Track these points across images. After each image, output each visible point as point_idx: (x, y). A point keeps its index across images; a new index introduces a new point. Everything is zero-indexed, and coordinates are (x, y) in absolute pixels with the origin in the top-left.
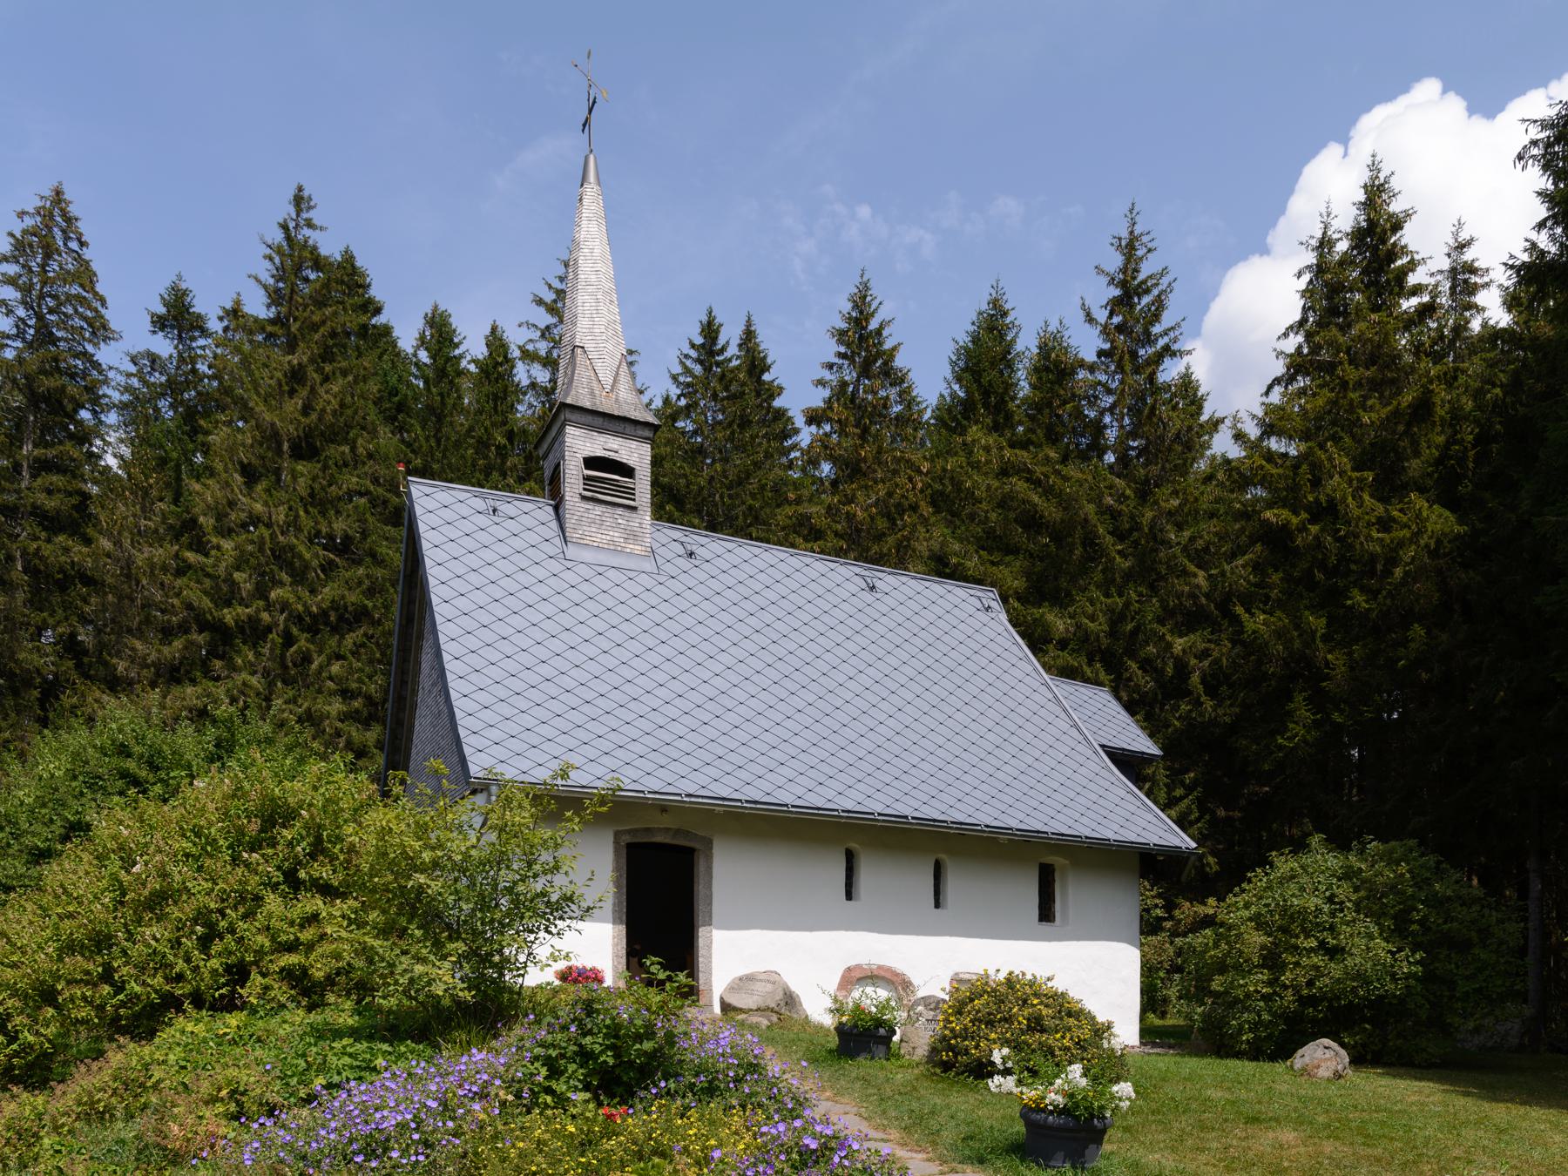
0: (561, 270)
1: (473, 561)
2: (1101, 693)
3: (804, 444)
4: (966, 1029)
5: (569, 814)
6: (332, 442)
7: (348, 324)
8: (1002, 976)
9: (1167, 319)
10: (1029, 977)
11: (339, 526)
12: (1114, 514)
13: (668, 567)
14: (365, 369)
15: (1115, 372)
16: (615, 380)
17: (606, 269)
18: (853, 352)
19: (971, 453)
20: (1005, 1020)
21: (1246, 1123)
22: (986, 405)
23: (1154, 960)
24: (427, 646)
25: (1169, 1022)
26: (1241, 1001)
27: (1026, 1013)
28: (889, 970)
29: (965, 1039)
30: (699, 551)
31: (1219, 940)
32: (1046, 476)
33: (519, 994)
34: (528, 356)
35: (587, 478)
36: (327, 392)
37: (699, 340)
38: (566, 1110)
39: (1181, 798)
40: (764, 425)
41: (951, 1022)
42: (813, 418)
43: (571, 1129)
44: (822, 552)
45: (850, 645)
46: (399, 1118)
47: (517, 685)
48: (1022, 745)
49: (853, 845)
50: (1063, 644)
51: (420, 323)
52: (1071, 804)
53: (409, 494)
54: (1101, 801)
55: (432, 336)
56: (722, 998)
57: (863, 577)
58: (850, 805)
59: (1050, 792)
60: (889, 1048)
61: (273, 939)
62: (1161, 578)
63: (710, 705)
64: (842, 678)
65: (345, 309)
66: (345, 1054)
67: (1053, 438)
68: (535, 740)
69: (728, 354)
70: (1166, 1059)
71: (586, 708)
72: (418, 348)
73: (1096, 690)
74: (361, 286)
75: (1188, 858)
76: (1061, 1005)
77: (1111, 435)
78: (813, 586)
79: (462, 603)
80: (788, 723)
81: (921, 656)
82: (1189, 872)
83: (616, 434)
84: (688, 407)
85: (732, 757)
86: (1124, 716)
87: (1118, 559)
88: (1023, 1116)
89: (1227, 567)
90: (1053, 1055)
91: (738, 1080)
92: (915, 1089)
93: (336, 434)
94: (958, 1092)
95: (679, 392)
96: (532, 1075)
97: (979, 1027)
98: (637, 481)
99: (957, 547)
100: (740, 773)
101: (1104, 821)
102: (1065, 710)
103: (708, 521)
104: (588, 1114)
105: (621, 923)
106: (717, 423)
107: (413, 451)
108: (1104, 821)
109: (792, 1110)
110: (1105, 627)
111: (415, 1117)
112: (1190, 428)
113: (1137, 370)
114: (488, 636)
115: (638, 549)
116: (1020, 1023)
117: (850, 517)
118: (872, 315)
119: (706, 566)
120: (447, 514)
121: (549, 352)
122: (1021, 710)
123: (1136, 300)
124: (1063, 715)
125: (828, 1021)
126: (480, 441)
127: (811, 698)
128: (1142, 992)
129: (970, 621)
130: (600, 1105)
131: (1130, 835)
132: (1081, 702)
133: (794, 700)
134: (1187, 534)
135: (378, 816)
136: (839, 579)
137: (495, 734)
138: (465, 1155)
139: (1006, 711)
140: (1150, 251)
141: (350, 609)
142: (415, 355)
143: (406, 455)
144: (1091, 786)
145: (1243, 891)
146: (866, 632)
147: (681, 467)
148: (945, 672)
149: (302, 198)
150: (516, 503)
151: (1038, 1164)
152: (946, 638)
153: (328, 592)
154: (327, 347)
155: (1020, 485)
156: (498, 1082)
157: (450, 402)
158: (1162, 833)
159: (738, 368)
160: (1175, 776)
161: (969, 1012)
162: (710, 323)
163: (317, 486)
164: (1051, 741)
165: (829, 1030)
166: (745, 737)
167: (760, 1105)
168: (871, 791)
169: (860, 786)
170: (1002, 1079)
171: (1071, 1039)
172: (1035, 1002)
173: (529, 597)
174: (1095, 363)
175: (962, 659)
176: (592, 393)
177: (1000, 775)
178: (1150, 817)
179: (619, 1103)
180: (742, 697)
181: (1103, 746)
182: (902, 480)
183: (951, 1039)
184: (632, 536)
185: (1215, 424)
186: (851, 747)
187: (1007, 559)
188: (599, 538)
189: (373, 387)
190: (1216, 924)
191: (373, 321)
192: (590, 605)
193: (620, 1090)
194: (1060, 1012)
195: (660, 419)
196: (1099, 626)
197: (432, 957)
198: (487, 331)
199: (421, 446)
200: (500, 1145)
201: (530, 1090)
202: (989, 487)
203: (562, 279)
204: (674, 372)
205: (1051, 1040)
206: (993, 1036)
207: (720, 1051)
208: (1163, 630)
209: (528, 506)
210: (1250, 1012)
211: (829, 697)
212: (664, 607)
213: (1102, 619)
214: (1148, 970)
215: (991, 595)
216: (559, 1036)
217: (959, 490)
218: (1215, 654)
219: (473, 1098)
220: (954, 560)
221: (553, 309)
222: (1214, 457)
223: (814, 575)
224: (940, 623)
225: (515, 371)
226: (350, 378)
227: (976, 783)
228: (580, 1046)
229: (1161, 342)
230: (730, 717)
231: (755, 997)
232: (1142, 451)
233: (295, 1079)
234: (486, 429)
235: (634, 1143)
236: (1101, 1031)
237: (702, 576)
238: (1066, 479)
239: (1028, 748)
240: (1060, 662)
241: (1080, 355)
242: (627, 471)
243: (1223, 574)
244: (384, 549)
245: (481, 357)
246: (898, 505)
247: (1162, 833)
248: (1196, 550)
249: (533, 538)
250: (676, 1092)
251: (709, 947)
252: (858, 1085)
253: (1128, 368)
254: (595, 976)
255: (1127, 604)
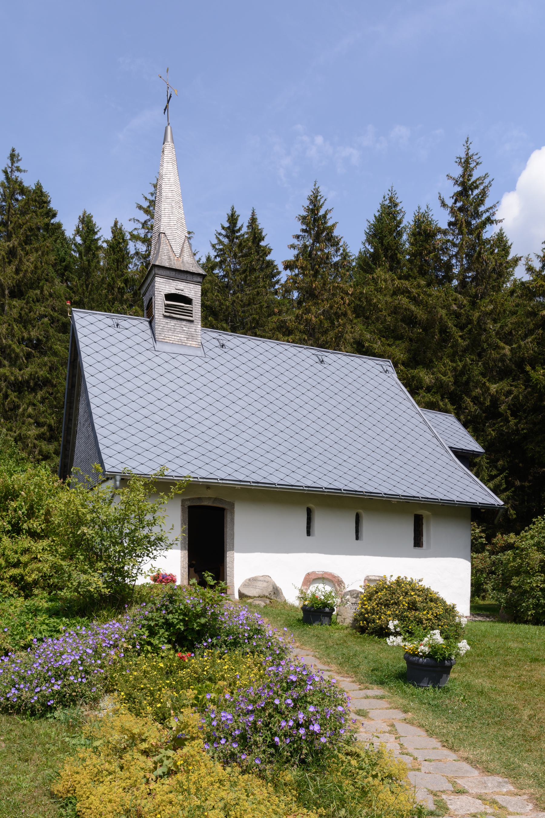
0: (152, 190)
1: (106, 353)
2: (450, 418)
3: (283, 281)
4: (373, 609)
5: (162, 494)
6: (31, 288)
7: (39, 224)
8: (394, 579)
9: (488, 203)
10: (409, 579)
11: (34, 333)
12: (458, 315)
13: (211, 354)
14: (48, 247)
15: (458, 234)
16: (182, 251)
17: (177, 189)
18: (310, 228)
19: (376, 283)
20: (396, 603)
21: (531, 662)
22: (386, 256)
23: (480, 566)
24: (82, 399)
25: (487, 602)
26: (528, 592)
27: (407, 600)
28: (330, 574)
29: (373, 614)
30: (227, 344)
31: (516, 557)
32: (419, 295)
33: (133, 590)
34: (135, 238)
35: (167, 306)
36: (28, 261)
37: (227, 225)
38: (158, 654)
39: (495, 476)
40: (262, 271)
41: (365, 605)
42: (288, 266)
43: (162, 665)
44: (293, 342)
45: (310, 394)
46: (73, 658)
47: (129, 420)
48: (405, 448)
49: (311, 505)
50: (428, 390)
51: (76, 222)
52: (432, 481)
53: (72, 318)
54: (449, 479)
55: (83, 228)
56: (239, 590)
57: (317, 355)
58: (309, 484)
59: (421, 474)
60: (331, 619)
61: (6, 561)
62: (484, 350)
63: (233, 429)
64: (305, 413)
65: (37, 215)
66: (44, 623)
67: (423, 273)
68: (140, 451)
69: (242, 232)
70: (485, 624)
71: (166, 432)
72: (75, 235)
73: (447, 415)
74: (45, 202)
75: (499, 510)
76: (427, 595)
77: (456, 271)
78: (289, 361)
79: (100, 376)
80: (275, 439)
81: (349, 399)
82: (499, 519)
83: (182, 280)
84: (221, 262)
85: (245, 458)
86: (462, 430)
87: (460, 340)
88: (405, 658)
89: (522, 343)
90: (422, 623)
91: (249, 638)
92: (345, 642)
93: (33, 284)
94: (369, 643)
95: (216, 254)
96: (140, 635)
97: (381, 607)
98: (194, 306)
99: (368, 336)
100: (249, 467)
101: (451, 491)
102: (429, 428)
103: (232, 326)
104: (170, 657)
105: (185, 550)
106: (236, 270)
107: (74, 292)
108: (451, 491)
109: (279, 654)
110: (452, 379)
111: (80, 657)
112: (501, 264)
113: (470, 233)
114: (115, 394)
115: (194, 344)
116: (403, 605)
117: (308, 322)
118: (321, 207)
119: (231, 352)
120: (93, 328)
121: (146, 235)
122: (405, 428)
123: (470, 193)
124: (428, 430)
125: (297, 603)
126: (109, 285)
127: (288, 424)
128: (472, 585)
129: (376, 378)
130: (176, 651)
131: (466, 498)
132: (438, 423)
133: (279, 426)
134: (499, 325)
135: (64, 496)
136: (304, 357)
137: (118, 448)
138: (106, 678)
139: (396, 429)
140: (477, 164)
141: (41, 379)
142: (74, 239)
143: (70, 294)
144: (444, 470)
145: (530, 529)
146: (319, 386)
147: (217, 296)
148: (362, 408)
149: (14, 155)
150: (129, 320)
151: (414, 685)
152: (363, 389)
153: (28, 370)
154: (27, 236)
155: (404, 301)
156: (123, 640)
157: (93, 264)
158: (484, 497)
159: (248, 239)
160: (493, 463)
161: (375, 600)
162: (233, 215)
163: (23, 313)
164: (421, 445)
165: (297, 608)
166: (252, 447)
167: (262, 652)
168: (321, 476)
169: (315, 473)
170: (394, 639)
171: (432, 614)
172: (413, 593)
173: (136, 372)
174: (446, 229)
175: (371, 400)
176: (169, 258)
177: (392, 465)
178: (477, 487)
179: (186, 650)
180: (251, 424)
181: (450, 448)
182: (338, 299)
183: (365, 614)
184: (191, 337)
185: (516, 261)
186: (310, 451)
187: (398, 342)
188: (174, 338)
189: (52, 258)
190: (514, 548)
191: (52, 221)
192: (168, 375)
193: (187, 643)
194: (426, 599)
195: (205, 270)
196: (448, 379)
197: (90, 571)
198: (112, 224)
199: (78, 289)
200: (124, 673)
201: (139, 643)
202: (386, 302)
203: (152, 194)
204: (213, 243)
205: (421, 615)
206: (389, 613)
207: (240, 622)
208: (484, 380)
209: (135, 322)
210: (533, 598)
211: (298, 423)
212: (208, 375)
213: (450, 374)
214: (476, 572)
215: (388, 363)
216: (155, 614)
217: (370, 305)
218: (515, 393)
219: (110, 648)
220: (367, 344)
221: (147, 211)
222: (515, 280)
223: (290, 355)
224: (360, 380)
225: (128, 247)
226: (40, 253)
227: (379, 470)
228: (166, 619)
229: (485, 216)
230: (244, 435)
231: (257, 590)
232: (474, 278)
233: (18, 637)
234: (113, 278)
235: (196, 673)
236: (450, 611)
237: (228, 357)
238: (430, 295)
239: (408, 450)
240: (427, 399)
241: (439, 226)
242: (188, 301)
243: (520, 347)
244: (58, 347)
245: (110, 239)
246: (336, 313)
247: (484, 497)
248: (505, 333)
249: (138, 339)
250: (217, 644)
251: (233, 562)
252: (314, 639)
253: (465, 230)
254: (170, 579)
255: (464, 366)
